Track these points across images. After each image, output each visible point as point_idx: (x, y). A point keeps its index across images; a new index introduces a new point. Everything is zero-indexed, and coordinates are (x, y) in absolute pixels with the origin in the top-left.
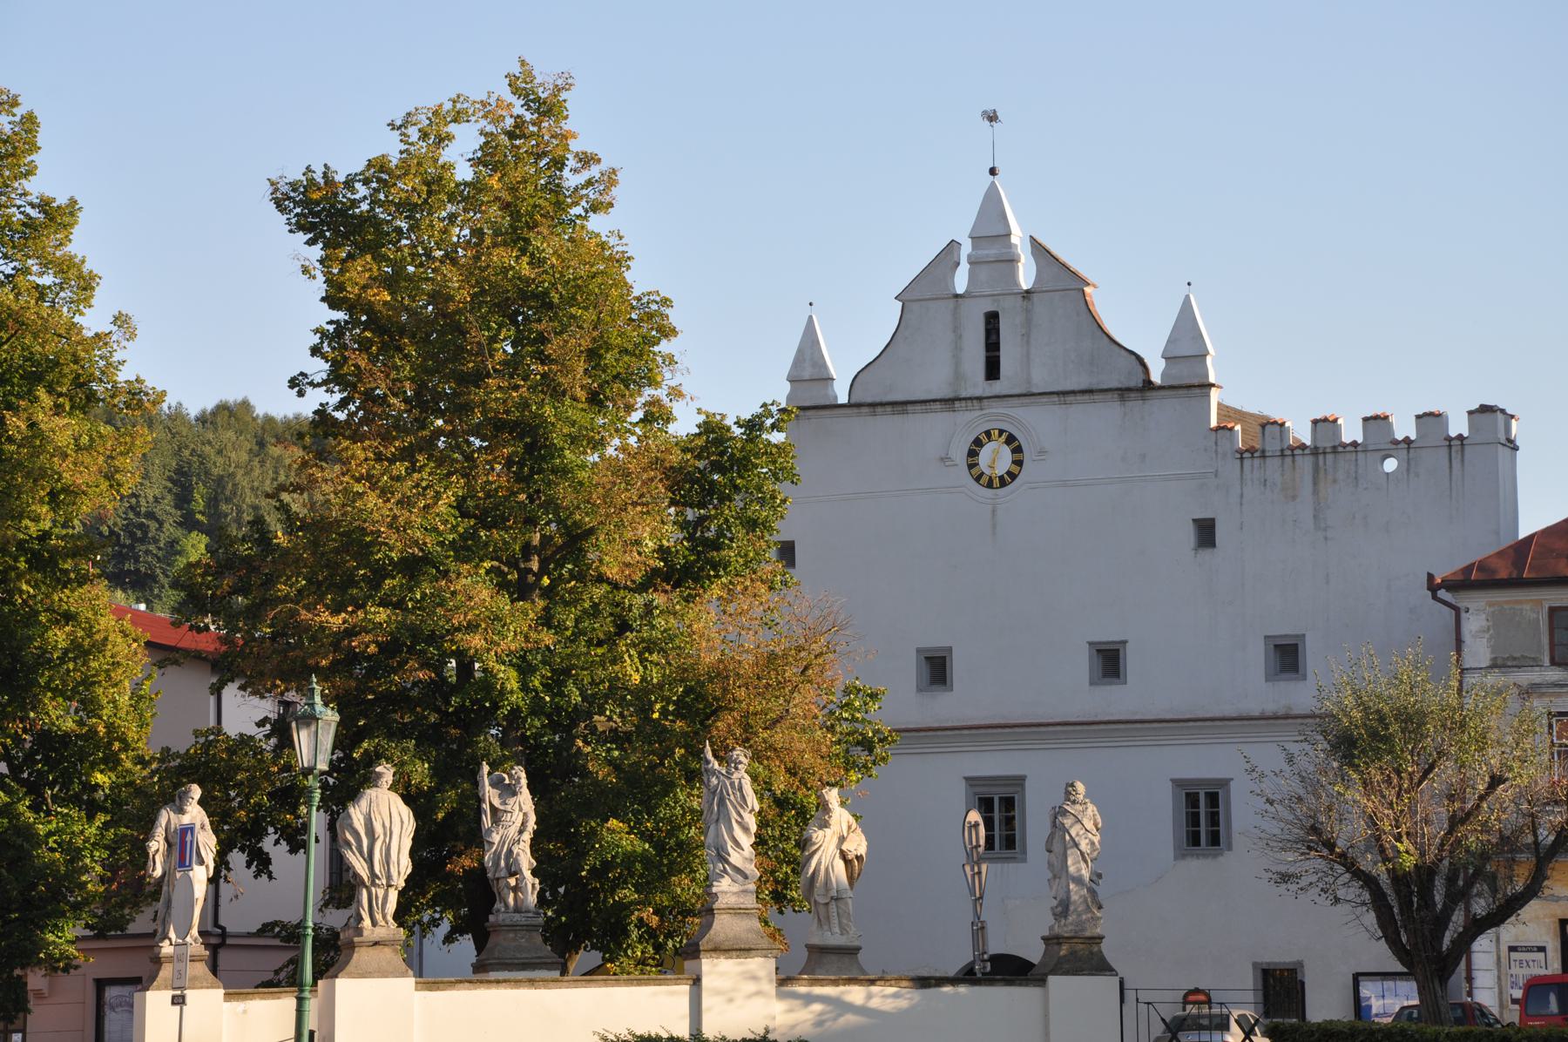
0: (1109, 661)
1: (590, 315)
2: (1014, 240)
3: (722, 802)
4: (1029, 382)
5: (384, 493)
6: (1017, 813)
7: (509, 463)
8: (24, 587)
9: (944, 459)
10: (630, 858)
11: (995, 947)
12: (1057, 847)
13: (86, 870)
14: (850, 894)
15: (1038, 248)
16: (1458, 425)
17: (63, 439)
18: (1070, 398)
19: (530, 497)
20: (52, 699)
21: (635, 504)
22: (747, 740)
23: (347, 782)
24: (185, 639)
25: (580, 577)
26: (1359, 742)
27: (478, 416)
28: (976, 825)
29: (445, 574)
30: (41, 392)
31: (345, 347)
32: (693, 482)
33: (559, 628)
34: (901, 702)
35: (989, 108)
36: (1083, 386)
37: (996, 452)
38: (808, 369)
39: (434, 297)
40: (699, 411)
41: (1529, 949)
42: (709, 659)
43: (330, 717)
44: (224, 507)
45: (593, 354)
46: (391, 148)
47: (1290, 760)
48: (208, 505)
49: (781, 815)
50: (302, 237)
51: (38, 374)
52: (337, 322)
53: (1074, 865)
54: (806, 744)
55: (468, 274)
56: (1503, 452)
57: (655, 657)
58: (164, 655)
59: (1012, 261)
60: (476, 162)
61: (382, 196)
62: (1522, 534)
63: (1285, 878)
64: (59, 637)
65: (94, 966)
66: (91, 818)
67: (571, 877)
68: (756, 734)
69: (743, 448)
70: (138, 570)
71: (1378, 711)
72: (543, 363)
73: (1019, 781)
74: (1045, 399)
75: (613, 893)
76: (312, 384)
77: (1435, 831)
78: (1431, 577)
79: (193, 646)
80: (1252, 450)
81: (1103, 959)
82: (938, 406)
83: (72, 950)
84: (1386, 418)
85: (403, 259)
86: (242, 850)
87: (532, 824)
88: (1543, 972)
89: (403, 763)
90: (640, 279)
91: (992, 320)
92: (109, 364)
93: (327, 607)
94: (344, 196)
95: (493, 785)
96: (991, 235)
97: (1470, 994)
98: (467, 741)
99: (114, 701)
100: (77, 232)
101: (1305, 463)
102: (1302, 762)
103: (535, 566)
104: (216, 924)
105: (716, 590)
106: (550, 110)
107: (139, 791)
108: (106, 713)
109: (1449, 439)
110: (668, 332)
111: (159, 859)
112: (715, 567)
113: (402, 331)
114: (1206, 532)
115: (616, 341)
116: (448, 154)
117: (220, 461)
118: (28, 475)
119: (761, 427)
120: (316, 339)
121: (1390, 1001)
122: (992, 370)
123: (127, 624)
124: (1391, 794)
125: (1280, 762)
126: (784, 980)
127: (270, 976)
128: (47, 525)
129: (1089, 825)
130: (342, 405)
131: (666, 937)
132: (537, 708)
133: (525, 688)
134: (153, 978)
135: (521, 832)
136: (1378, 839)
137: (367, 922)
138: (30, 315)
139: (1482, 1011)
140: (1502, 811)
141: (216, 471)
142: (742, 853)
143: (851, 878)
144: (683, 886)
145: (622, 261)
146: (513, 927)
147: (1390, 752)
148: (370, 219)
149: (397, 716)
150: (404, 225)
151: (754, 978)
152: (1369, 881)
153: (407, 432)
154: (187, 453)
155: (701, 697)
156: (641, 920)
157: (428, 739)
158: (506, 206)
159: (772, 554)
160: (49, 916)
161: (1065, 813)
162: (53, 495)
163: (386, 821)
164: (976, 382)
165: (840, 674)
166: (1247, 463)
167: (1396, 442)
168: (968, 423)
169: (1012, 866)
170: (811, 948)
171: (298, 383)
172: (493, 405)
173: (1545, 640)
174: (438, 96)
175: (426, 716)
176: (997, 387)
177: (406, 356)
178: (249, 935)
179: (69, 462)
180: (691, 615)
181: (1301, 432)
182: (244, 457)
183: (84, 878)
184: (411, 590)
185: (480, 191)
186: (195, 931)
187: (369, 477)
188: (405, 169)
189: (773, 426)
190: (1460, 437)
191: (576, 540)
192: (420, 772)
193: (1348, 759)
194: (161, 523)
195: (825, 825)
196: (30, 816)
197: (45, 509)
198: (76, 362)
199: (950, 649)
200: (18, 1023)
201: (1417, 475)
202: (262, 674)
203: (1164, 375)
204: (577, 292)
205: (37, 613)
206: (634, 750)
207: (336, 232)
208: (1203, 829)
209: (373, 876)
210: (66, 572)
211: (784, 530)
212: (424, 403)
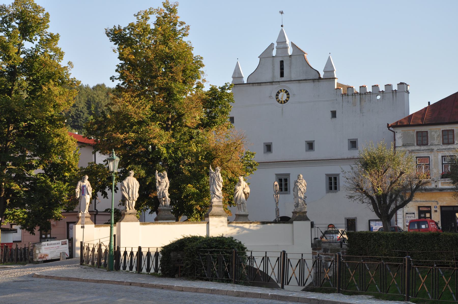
0: (310, 146)
1: (183, 62)
2: (287, 43)
3: (214, 180)
4: (291, 77)
5: (133, 105)
6: (288, 182)
7: (164, 98)
8: (48, 128)
9: (270, 97)
10: (193, 194)
11: (281, 215)
12: (296, 190)
13: (64, 196)
14: (246, 202)
15: (293, 45)
16: (395, 88)
17: (56, 92)
18: (301, 82)
19: (169, 106)
20: (55, 155)
21: (194, 108)
22: (222, 165)
23: (123, 176)
24: (86, 141)
25: (181, 125)
26: (369, 164)
27: (156, 87)
28: (277, 185)
29: (148, 125)
30: (51, 81)
31: (123, 69)
32: (208, 102)
33: (176, 138)
34: (260, 156)
35: (281, 10)
36: (304, 79)
37: (283, 95)
38: (237, 75)
39: (145, 57)
40: (210, 85)
41: (411, 214)
42: (213, 145)
43: (117, 159)
44: (99, 110)
45: (184, 71)
46: (134, 21)
47: (352, 169)
48: (95, 109)
49: (230, 183)
50: (113, 43)
51: (50, 76)
52: (122, 64)
53: (300, 194)
54: (236, 166)
55: (153, 51)
56: (406, 94)
57: (199, 145)
58: (81, 145)
59: (287, 48)
60: (155, 24)
61: (132, 33)
62: (410, 114)
63: (351, 197)
64: (56, 140)
65: (66, 219)
66: (64, 184)
67: (179, 198)
68: (224, 163)
69: (220, 94)
70: (78, 125)
71: (373, 157)
72: (171, 73)
73: (289, 175)
74: (295, 82)
75: (189, 201)
76: (116, 79)
77: (388, 185)
78: (388, 124)
79: (88, 142)
80: (345, 94)
81: (307, 217)
82: (269, 84)
83: (61, 215)
84: (378, 86)
85: (138, 48)
86: (100, 191)
87: (168, 185)
88: (414, 219)
89: (138, 171)
90: (195, 53)
91: (282, 62)
92: (67, 74)
93: (120, 133)
94: (124, 33)
95: (159, 176)
96: (282, 41)
97: (396, 224)
98: (154, 165)
99: (70, 156)
100: (59, 42)
101: (358, 97)
102: (355, 169)
103: (170, 123)
104: (95, 209)
105: (214, 129)
106: (173, 11)
107: (76, 177)
108: (68, 158)
109: (393, 91)
110: (202, 66)
111: (78, 193)
112: (214, 123)
113: (138, 66)
114: (334, 114)
115: (189, 68)
116: (148, 22)
117: (98, 98)
118: (48, 101)
119: (225, 89)
120: (117, 68)
121: (377, 226)
122: (282, 75)
123: (72, 137)
124: (377, 177)
125: (350, 169)
126: (229, 222)
127: (107, 222)
128: (53, 113)
129: (303, 185)
130: (123, 84)
131: (203, 212)
132: (171, 157)
133: (168, 153)
134: (78, 222)
135: (166, 187)
136: (373, 187)
137: (128, 209)
138: (48, 62)
139: (399, 228)
140: (404, 180)
141: (97, 101)
142: (219, 191)
143: (246, 198)
144: (206, 200)
145: (191, 48)
146: (164, 210)
147: (376, 166)
148: (129, 38)
149: (137, 159)
150: (138, 40)
151: (222, 222)
152: (371, 198)
153: (139, 90)
154: (90, 96)
155: (211, 155)
156: (196, 208)
157: (144, 165)
158: (162, 35)
159: (228, 120)
160: (55, 207)
161: (298, 182)
162: (54, 106)
163: (132, 184)
164: (278, 78)
165: (244, 149)
166: (344, 97)
167: (380, 92)
168: (276, 88)
169: (287, 195)
170: (236, 215)
171: (112, 78)
172: (159, 84)
173: (415, 140)
174: (147, 8)
175: (140, 158)
176: (283, 79)
177: (139, 72)
178: (103, 212)
179: (58, 98)
180: (208, 135)
181: (357, 90)
182: (104, 97)
183: (63, 198)
184: (140, 129)
185: (156, 31)
186: (87, 211)
187: (129, 101)
188: (138, 26)
189: (228, 89)
190: (395, 90)
191: (180, 116)
192: (143, 173)
193: (366, 168)
194: (84, 114)
195: (240, 185)
196: (50, 183)
197: (52, 109)
198: (59, 74)
199: (272, 143)
200: (49, 232)
201: (385, 100)
202: (104, 149)
203: (324, 76)
204: (180, 56)
205: (51, 134)
206: (194, 168)
207: (121, 41)
208: (333, 186)
209: (129, 198)
210: (57, 124)
211: (231, 114)
212: (143, 83)
